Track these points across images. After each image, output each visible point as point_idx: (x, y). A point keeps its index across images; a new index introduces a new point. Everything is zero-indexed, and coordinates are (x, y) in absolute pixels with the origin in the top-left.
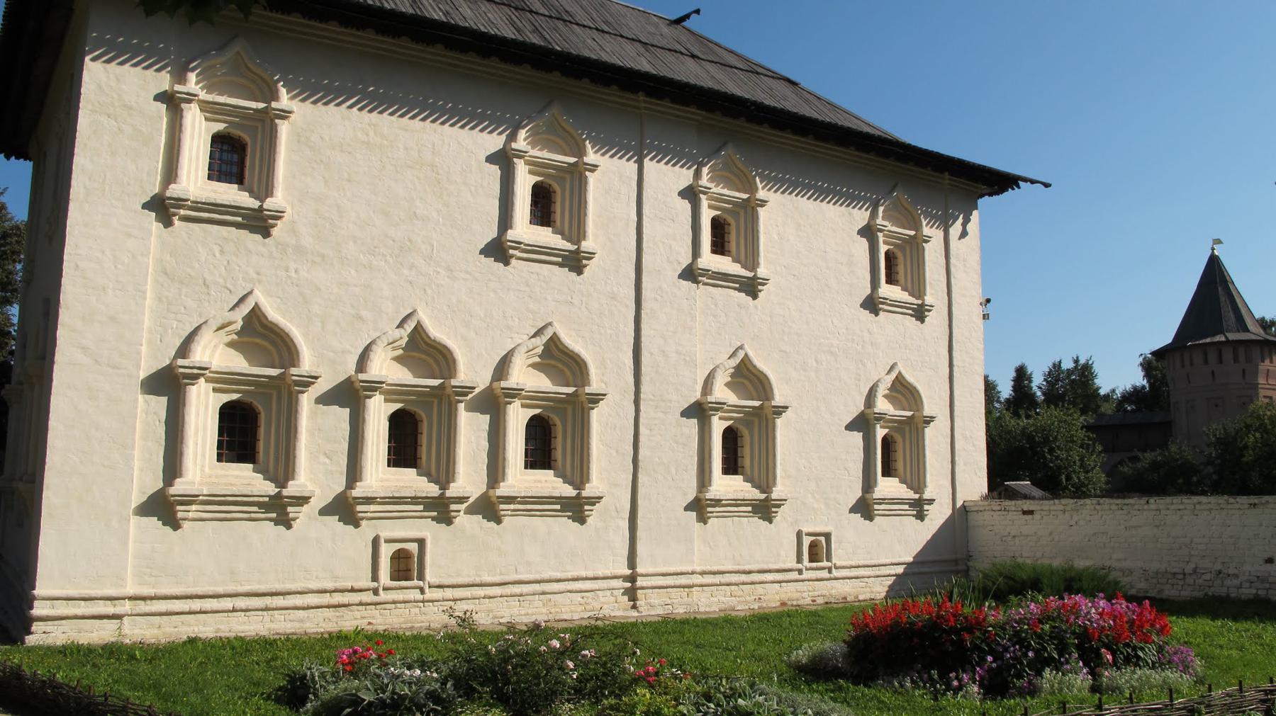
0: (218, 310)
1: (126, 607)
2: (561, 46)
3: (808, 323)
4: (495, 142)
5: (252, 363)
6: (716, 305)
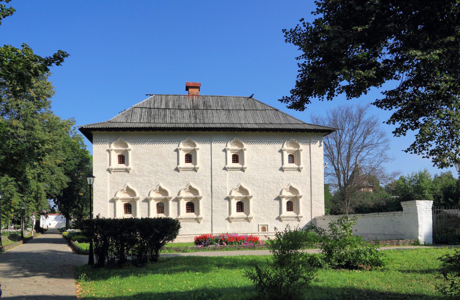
0: (184, 186)
3: (260, 176)
5: (130, 196)
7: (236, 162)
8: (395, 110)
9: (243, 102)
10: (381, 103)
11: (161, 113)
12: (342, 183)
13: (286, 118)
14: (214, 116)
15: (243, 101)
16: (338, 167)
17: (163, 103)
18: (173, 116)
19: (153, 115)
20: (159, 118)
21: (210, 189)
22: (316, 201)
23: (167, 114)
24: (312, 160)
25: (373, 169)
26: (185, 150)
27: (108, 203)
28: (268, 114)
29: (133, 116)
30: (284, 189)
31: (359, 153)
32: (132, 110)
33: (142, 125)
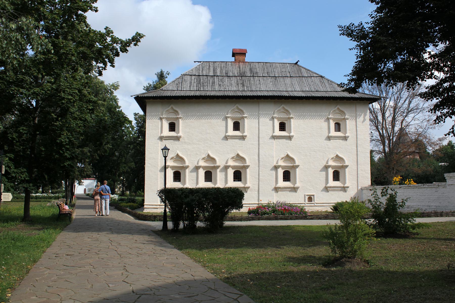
1: (158, 207)
2: (311, 89)
6: (280, 143)
7: (283, 131)
8: (435, 101)
9: (289, 68)
10: (424, 95)
11: (209, 81)
12: (387, 149)
13: (331, 85)
14: (261, 83)
15: (289, 67)
16: (383, 132)
17: (211, 70)
18: (221, 83)
19: (202, 82)
20: (208, 85)
21: (257, 158)
22: (362, 170)
23: (216, 81)
24: (358, 128)
25: (419, 135)
27: (159, 173)
28: (313, 81)
29: (183, 83)
30: (200, 160)
31: (404, 118)
32: (182, 77)
33: (192, 94)
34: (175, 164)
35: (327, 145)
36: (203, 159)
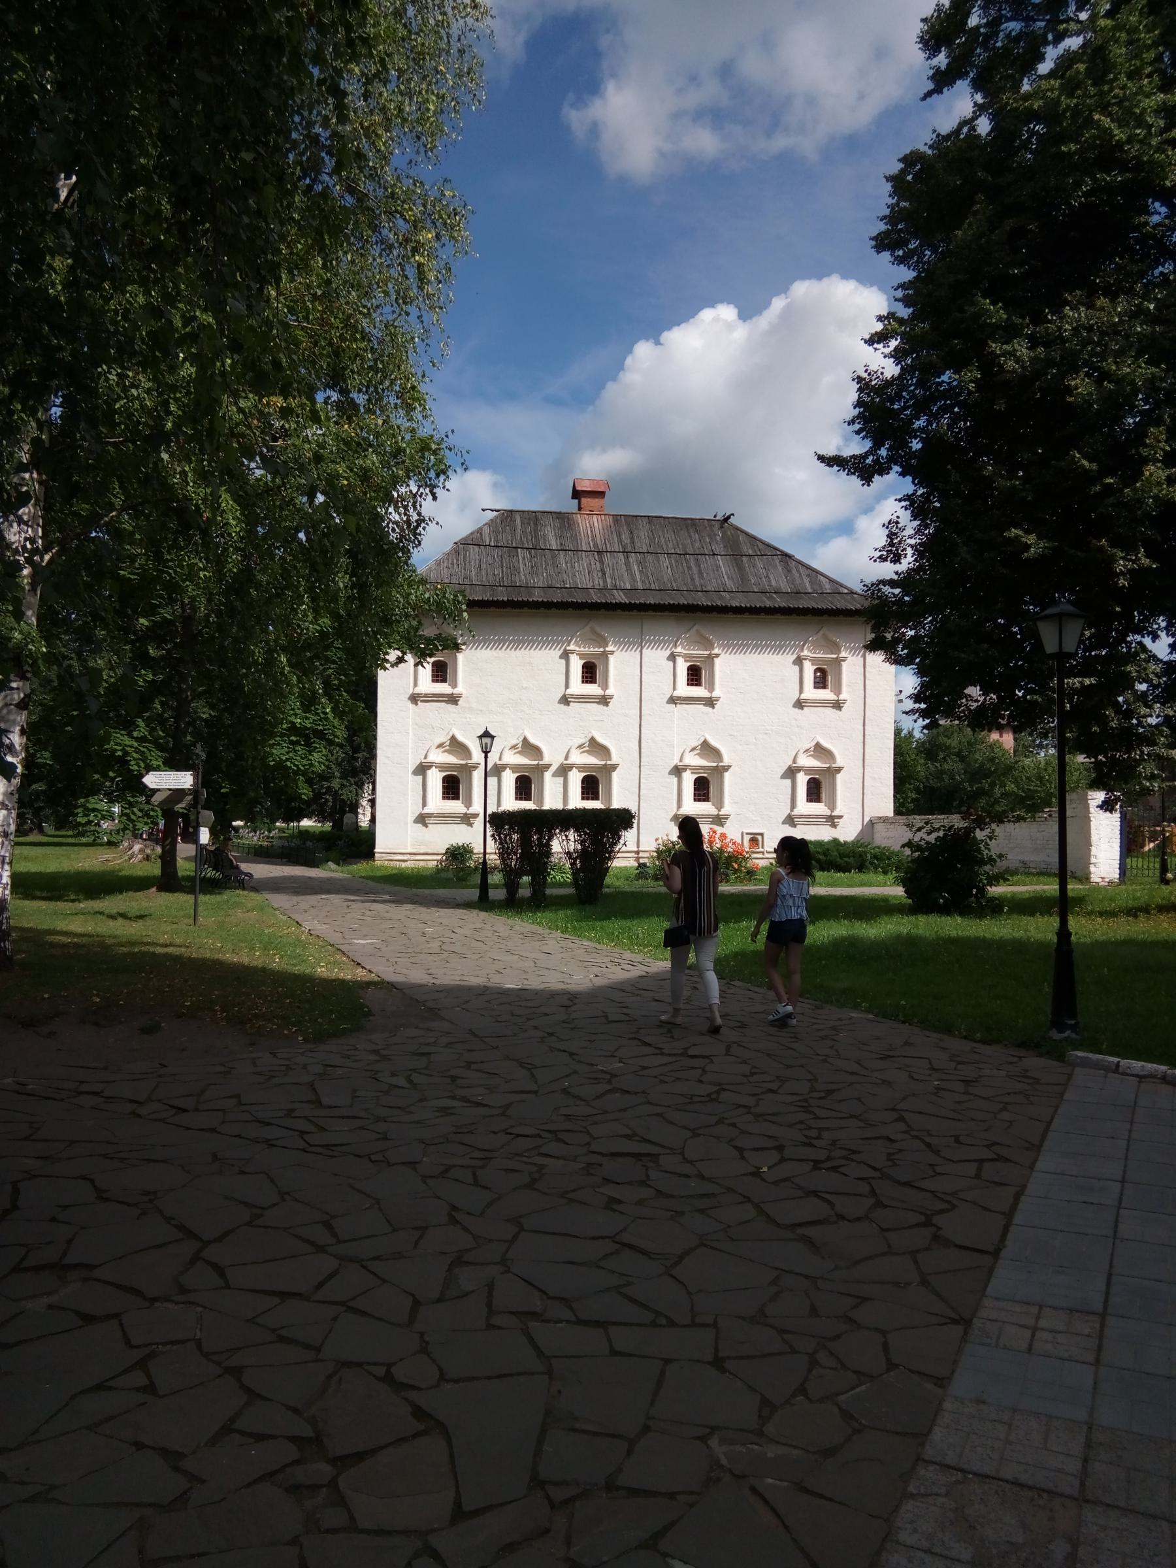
4: (668, 653)
22: (874, 778)
24: (867, 682)
26: (581, 656)
27: (410, 777)
30: (573, 748)
34: (704, 763)
35: (796, 720)
36: (514, 747)
